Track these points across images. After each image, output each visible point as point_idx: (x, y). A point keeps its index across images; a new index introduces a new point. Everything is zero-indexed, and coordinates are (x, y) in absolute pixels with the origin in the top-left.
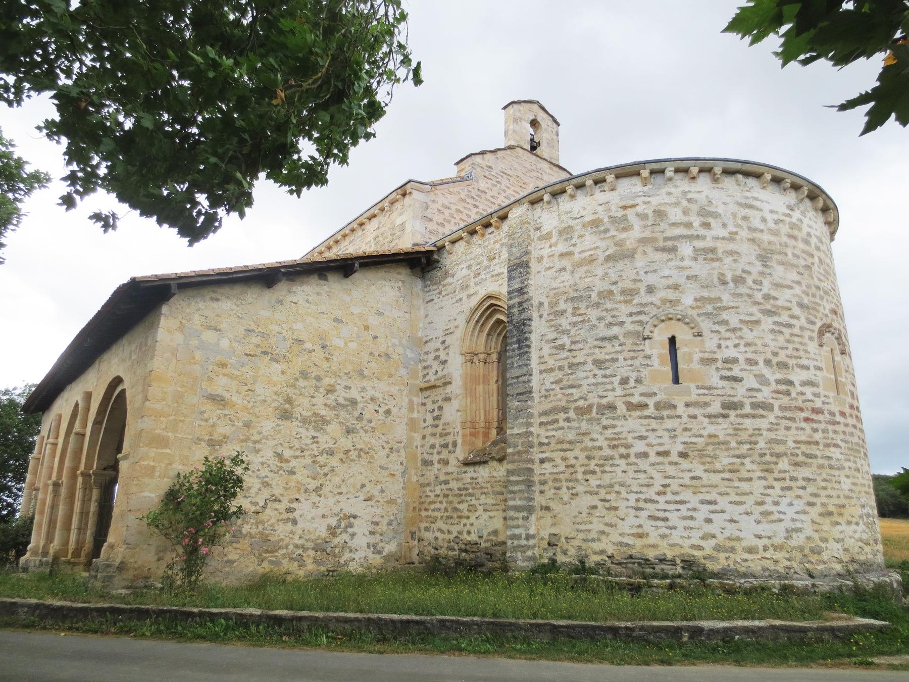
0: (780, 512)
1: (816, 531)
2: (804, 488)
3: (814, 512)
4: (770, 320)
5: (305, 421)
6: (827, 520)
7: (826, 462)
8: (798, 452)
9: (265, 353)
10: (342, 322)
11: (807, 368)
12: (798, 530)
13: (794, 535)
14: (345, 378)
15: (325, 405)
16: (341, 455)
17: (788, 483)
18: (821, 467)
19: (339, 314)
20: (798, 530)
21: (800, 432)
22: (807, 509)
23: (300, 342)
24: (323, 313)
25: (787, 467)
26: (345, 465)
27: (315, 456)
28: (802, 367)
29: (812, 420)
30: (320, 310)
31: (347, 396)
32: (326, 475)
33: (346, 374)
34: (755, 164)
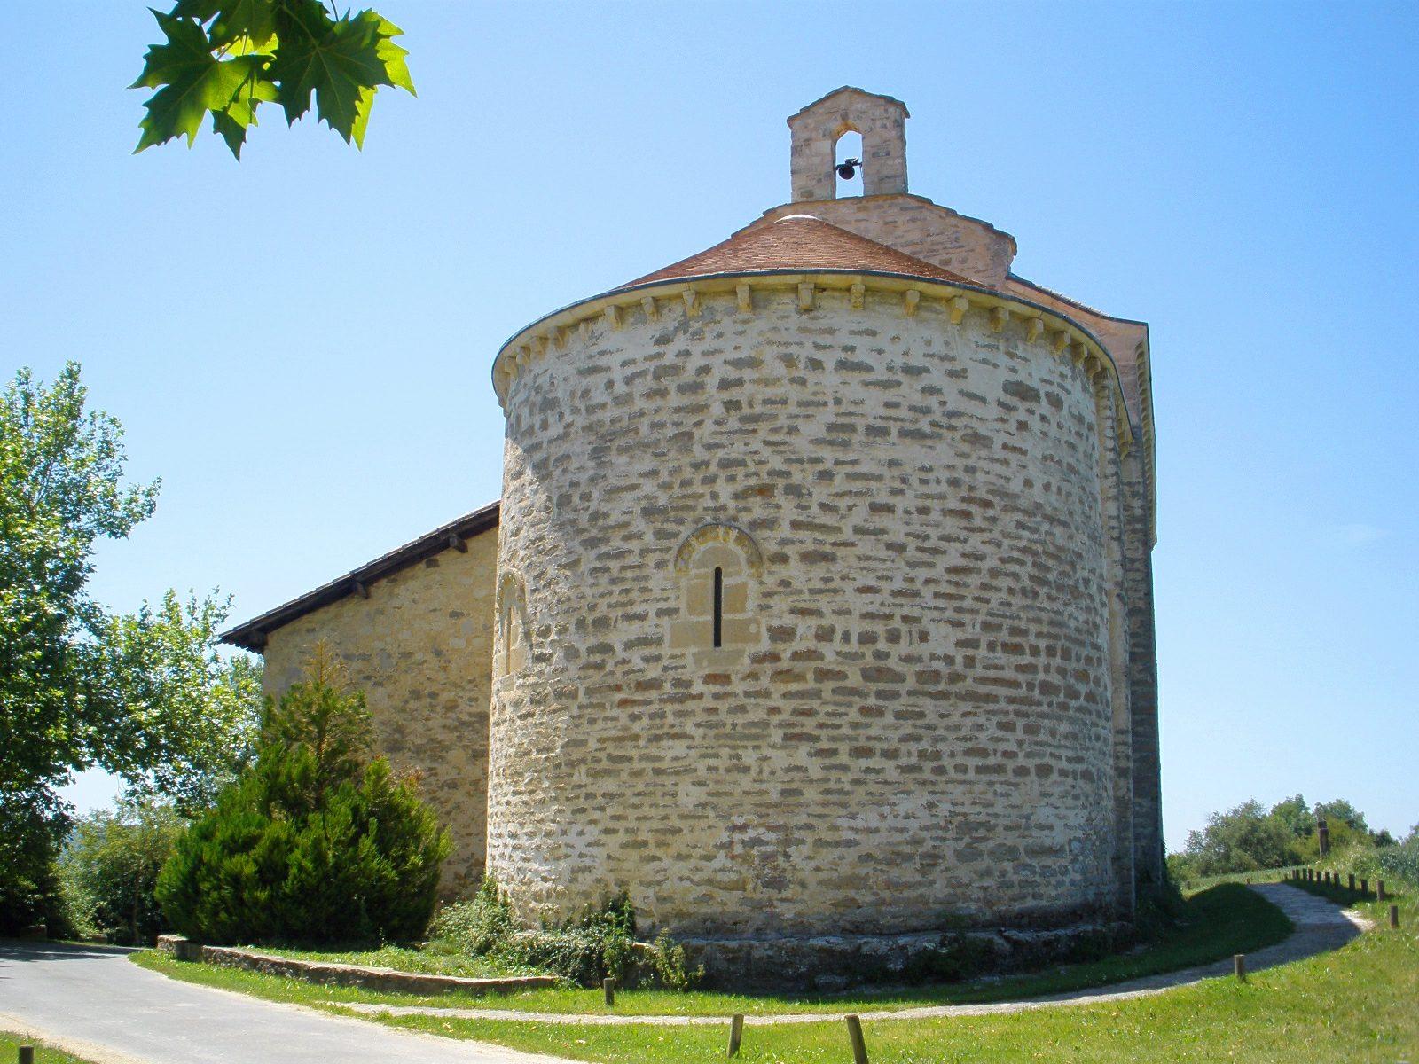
0: (567, 845)
1: (611, 871)
2: (602, 809)
3: (613, 842)
4: (593, 553)
5: (419, 750)
6: (634, 855)
7: (648, 766)
8: (602, 755)
9: (368, 678)
10: (462, 614)
11: (642, 617)
12: (588, 869)
13: (580, 876)
14: (469, 686)
15: (444, 727)
16: (468, 787)
17: (582, 803)
18: (637, 774)
19: (456, 605)
20: (588, 869)
21: (610, 724)
22: (604, 838)
23: (409, 655)
24: (435, 610)
25: (585, 780)
26: (474, 799)
27: (435, 792)
28: (629, 618)
29: (634, 703)
30: (431, 608)
31: (473, 710)
32: (448, 813)
33: (470, 682)
34: (582, 303)
